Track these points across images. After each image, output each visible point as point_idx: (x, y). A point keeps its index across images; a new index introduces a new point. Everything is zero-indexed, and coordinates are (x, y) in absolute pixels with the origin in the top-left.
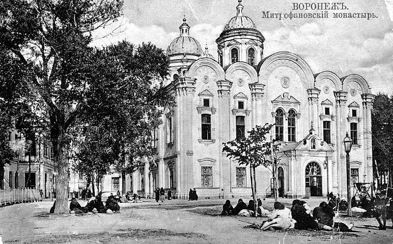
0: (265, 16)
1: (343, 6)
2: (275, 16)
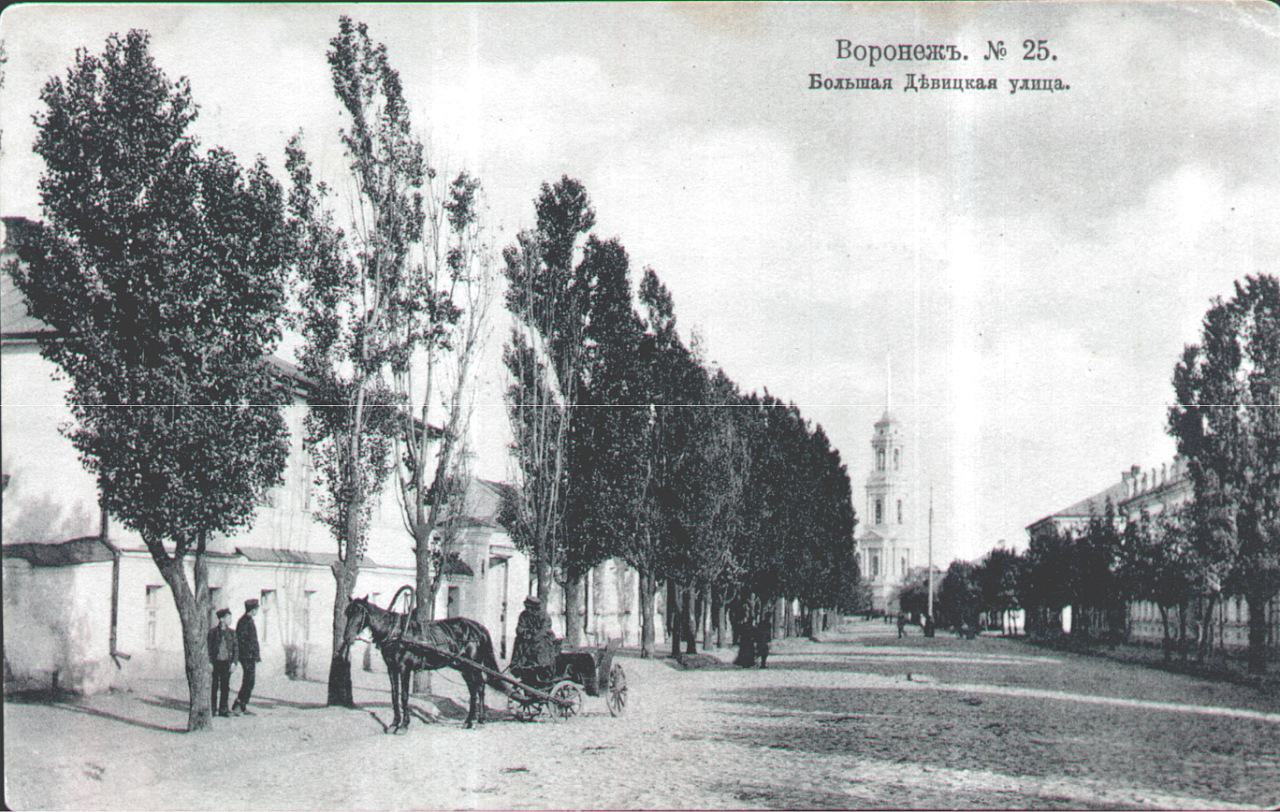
1: (953, 52)
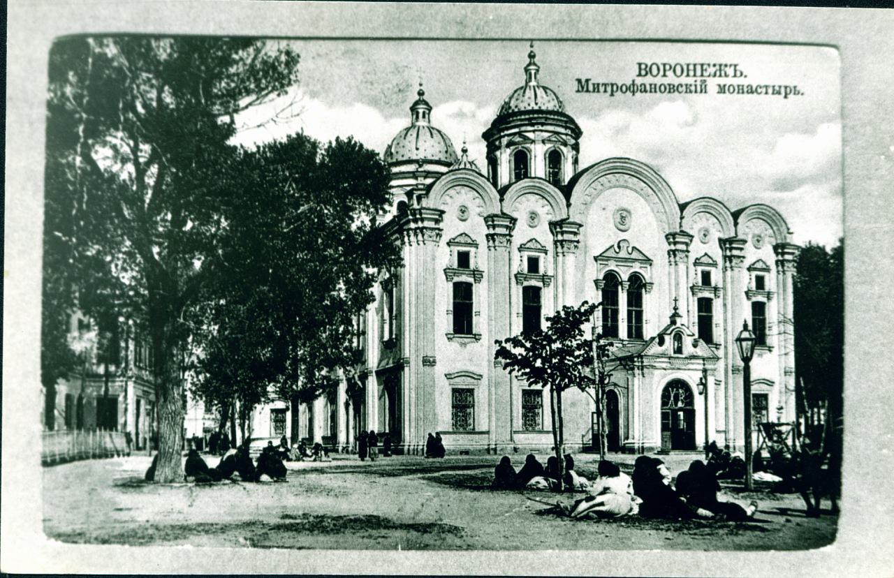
0: (583, 88)
1: (735, 71)
2: (602, 89)
